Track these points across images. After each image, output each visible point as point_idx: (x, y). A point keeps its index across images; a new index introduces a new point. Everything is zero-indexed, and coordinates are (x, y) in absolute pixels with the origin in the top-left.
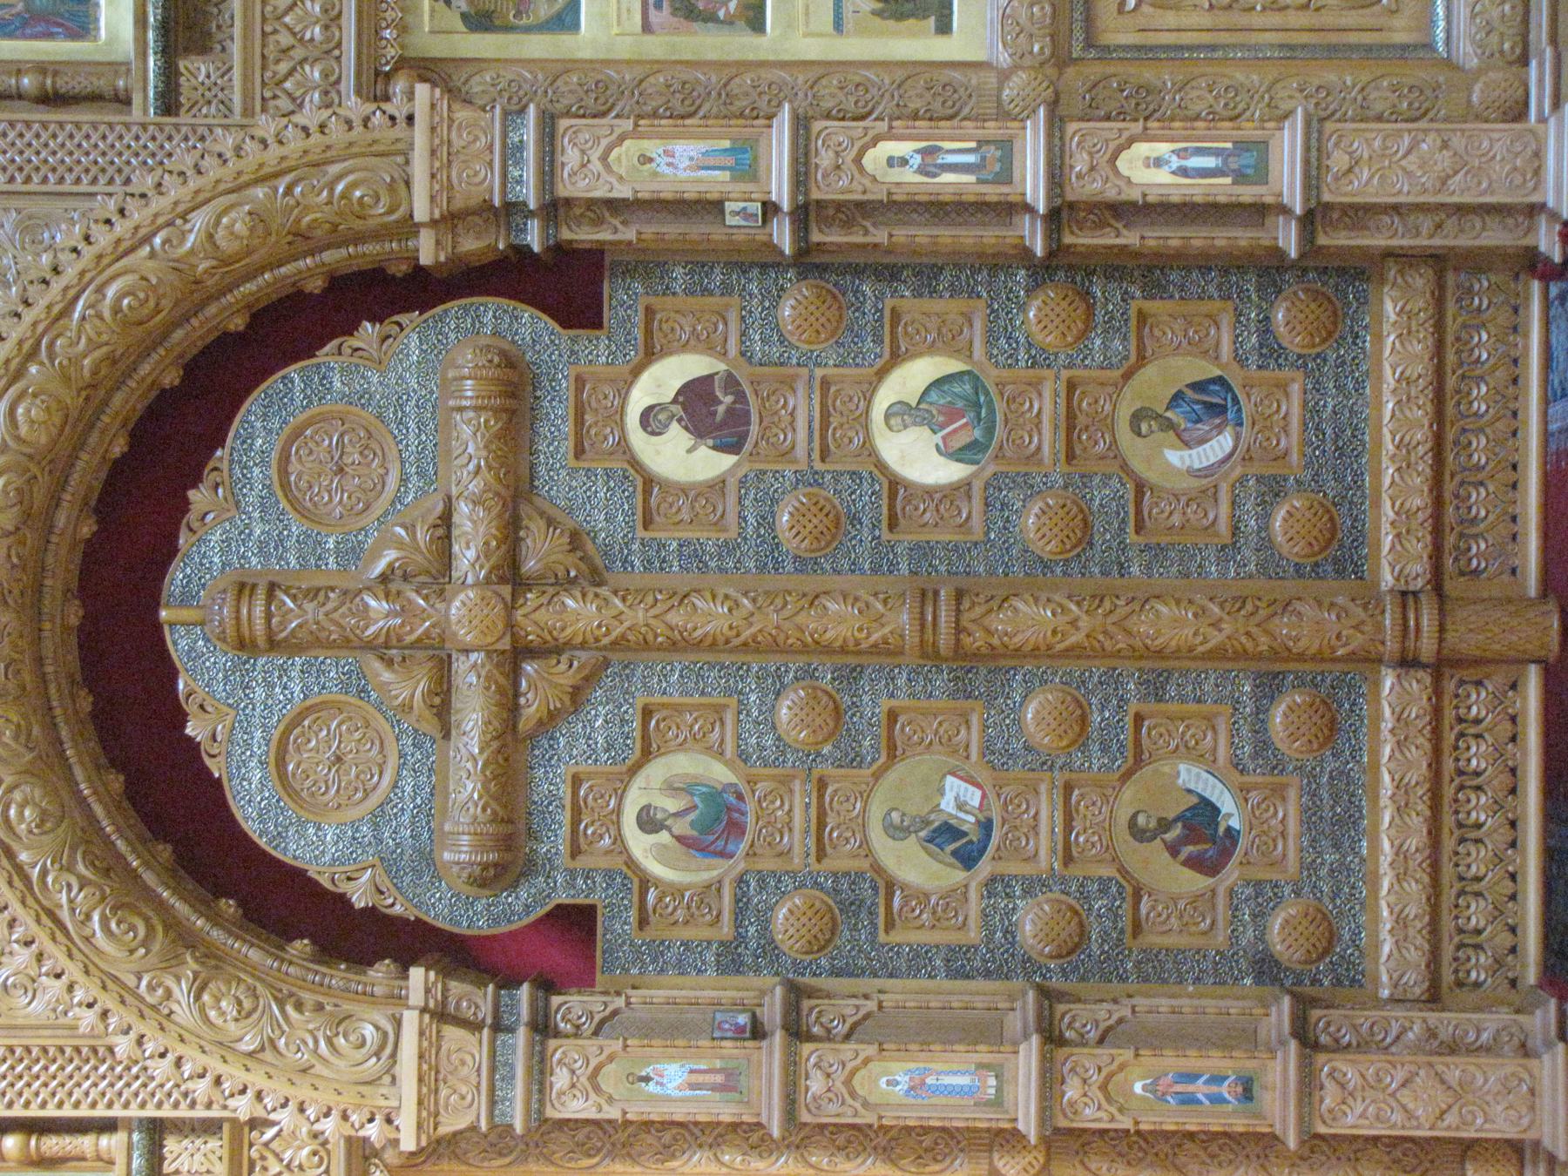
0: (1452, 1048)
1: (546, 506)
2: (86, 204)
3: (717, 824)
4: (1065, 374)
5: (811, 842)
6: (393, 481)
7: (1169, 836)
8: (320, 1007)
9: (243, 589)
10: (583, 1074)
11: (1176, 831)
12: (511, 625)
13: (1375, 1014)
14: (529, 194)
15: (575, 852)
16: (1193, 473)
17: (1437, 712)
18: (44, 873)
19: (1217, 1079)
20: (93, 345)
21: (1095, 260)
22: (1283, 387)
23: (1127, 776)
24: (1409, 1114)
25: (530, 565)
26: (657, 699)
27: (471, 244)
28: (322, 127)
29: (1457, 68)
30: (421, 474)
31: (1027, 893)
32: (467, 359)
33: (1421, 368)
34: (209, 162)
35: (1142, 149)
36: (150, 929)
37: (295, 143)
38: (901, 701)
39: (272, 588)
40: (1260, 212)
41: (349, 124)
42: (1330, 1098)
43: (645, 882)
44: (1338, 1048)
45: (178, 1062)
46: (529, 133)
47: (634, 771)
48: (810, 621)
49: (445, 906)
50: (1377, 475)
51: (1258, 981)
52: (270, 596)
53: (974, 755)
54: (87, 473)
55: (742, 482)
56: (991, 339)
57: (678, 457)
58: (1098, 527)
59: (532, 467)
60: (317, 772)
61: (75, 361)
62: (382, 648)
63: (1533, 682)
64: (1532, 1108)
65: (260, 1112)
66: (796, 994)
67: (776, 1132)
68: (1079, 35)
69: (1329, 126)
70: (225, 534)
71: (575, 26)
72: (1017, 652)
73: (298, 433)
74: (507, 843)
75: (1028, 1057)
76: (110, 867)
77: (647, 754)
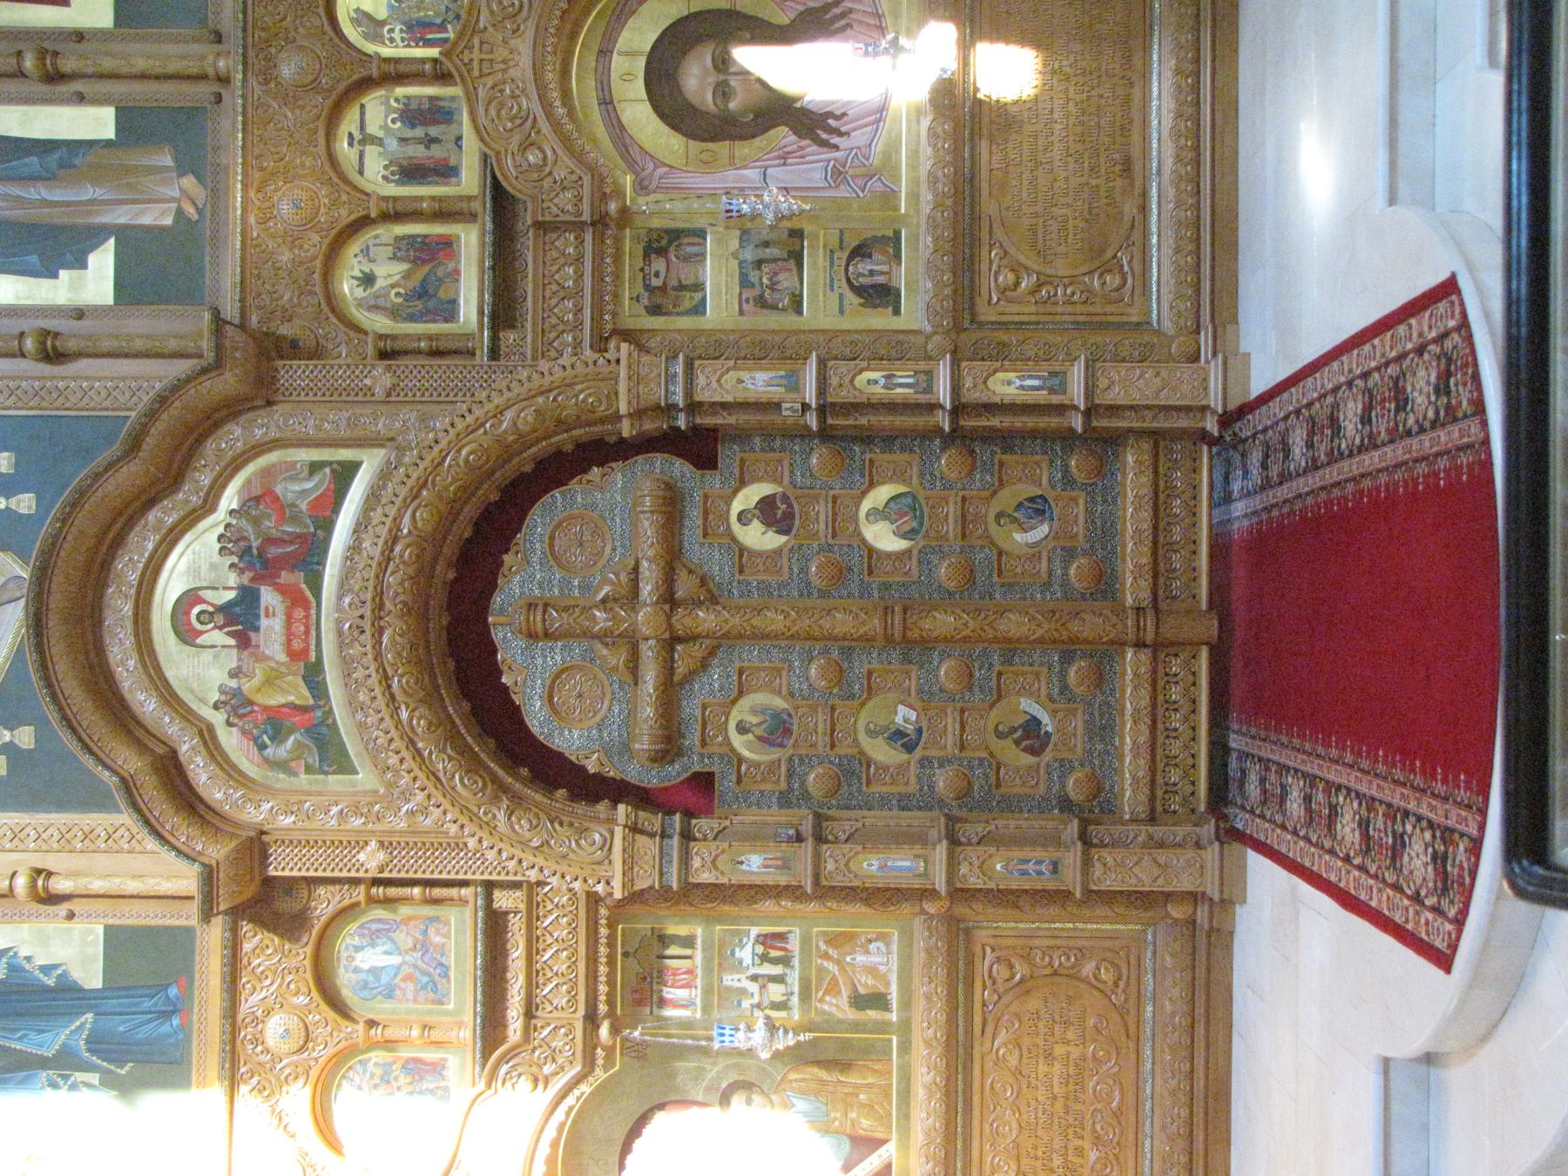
0: (1161, 845)
1: (689, 564)
2: (450, 407)
3: (778, 730)
4: (961, 494)
5: (827, 739)
6: (608, 549)
7: (1016, 736)
8: (571, 824)
9: (531, 606)
10: (708, 860)
11: (1019, 733)
12: (670, 625)
13: (1120, 828)
14: (679, 399)
15: (704, 743)
16: (1027, 545)
17: (1154, 671)
18: (431, 753)
19: (1040, 862)
20: (455, 480)
21: (977, 433)
22: (1074, 500)
23: (992, 706)
24: (1140, 880)
25: (680, 594)
26: (746, 664)
27: (649, 426)
28: (573, 366)
29: (1165, 335)
30: (623, 546)
31: (941, 766)
32: (647, 486)
33: (1146, 491)
34: (514, 385)
35: (1000, 375)
36: (485, 786)
37: (559, 374)
38: (875, 665)
39: (546, 605)
40: (1061, 409)
41: (587, 364)
42: (1098, 871)
43: (740, 760)
44: (1103, 845)
45: (500, 851)
46: (679, 369)
47: (734, 702)
48: (826, 623)
49: (635, 772)
50: (1124, 546)
51: (1062, 811)
52: (545, 612)
53: (913, 693)
54: (450, 550)
55: (791, 550)
56: (922, 475)
57: (758, 537)
58: (978, 575)
59: (681, 542)
60: (575, 703)
61: (446, 489)
62: (603, 636)
63: (1204, 654)
64: (1202, 875)
65: (541, 878)
66: (819, 818)
67: (809, 891)
68: (967, 316)
69: (1098, 365)
70: (522, 579)
71: (704, 313)
72: (936, 639)
73: (560, 524)
74: (668, 739)
75: (941, 851)
76: (464, 750)
77: (741, 694)
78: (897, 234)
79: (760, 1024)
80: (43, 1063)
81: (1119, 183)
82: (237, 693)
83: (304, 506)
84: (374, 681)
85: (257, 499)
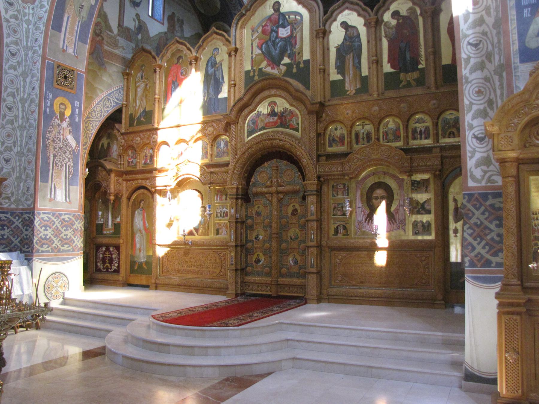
60: (263, 176)
70: (283, 164)
78: (348, 235)
79: (211, 213)
80: (208, 91)
81: (359, 280)
82: (260, 115)
83: (291, 123)
84: (259, 140)
85: (292, 114)
